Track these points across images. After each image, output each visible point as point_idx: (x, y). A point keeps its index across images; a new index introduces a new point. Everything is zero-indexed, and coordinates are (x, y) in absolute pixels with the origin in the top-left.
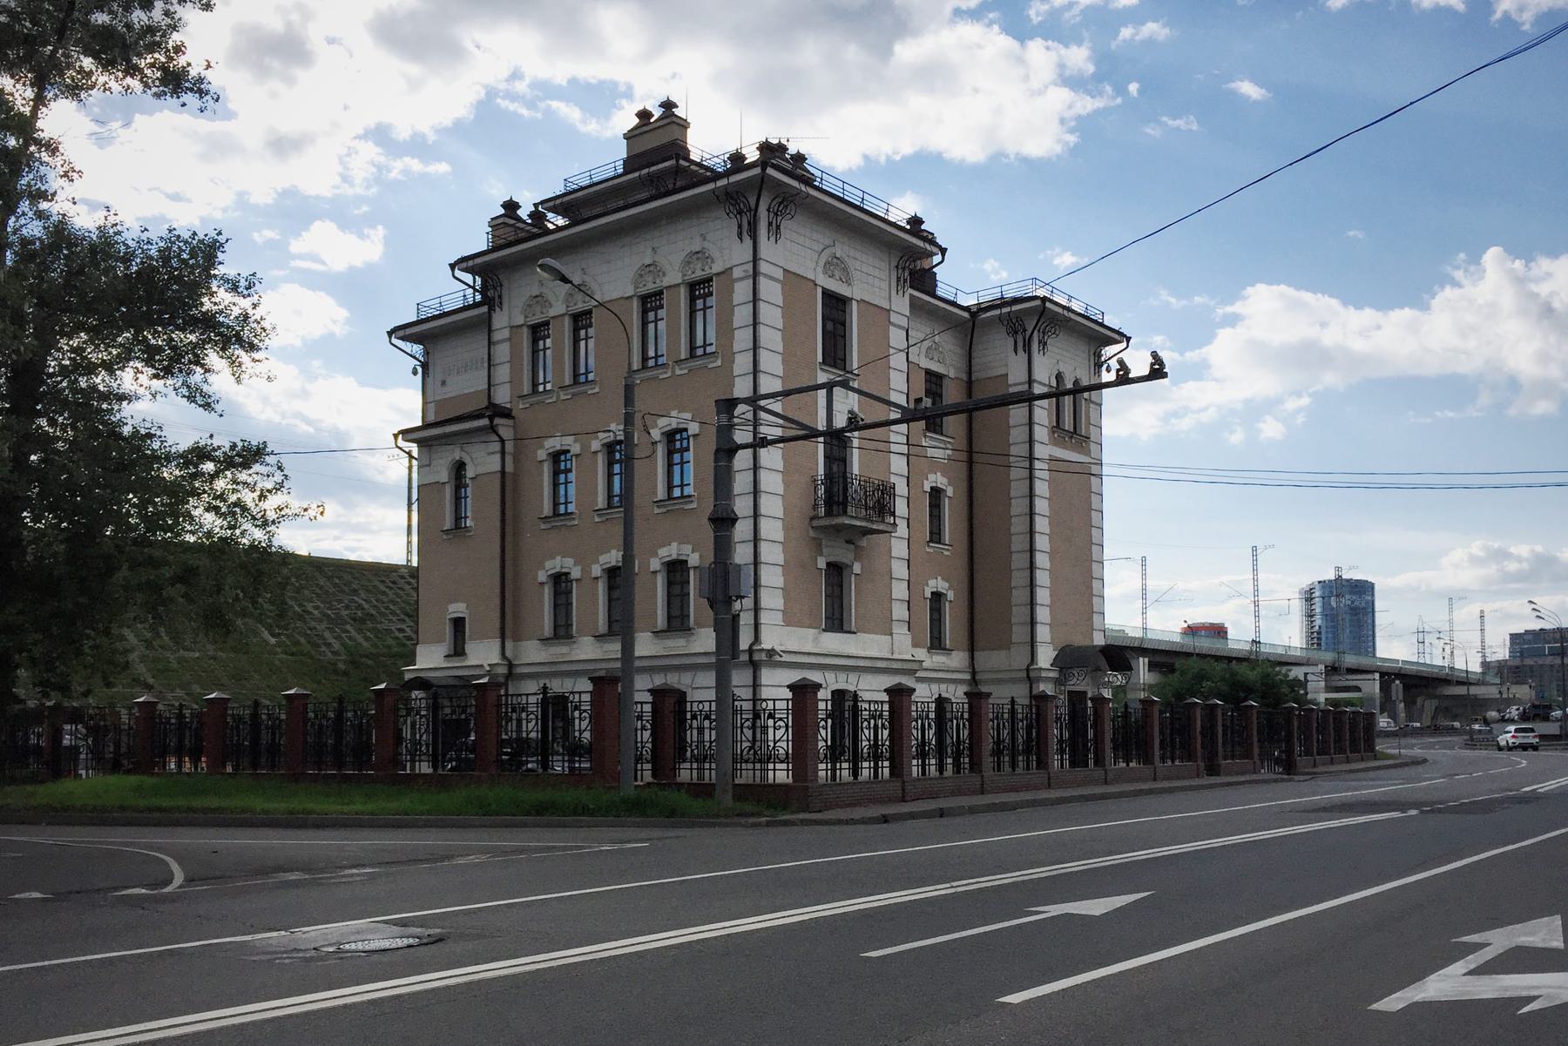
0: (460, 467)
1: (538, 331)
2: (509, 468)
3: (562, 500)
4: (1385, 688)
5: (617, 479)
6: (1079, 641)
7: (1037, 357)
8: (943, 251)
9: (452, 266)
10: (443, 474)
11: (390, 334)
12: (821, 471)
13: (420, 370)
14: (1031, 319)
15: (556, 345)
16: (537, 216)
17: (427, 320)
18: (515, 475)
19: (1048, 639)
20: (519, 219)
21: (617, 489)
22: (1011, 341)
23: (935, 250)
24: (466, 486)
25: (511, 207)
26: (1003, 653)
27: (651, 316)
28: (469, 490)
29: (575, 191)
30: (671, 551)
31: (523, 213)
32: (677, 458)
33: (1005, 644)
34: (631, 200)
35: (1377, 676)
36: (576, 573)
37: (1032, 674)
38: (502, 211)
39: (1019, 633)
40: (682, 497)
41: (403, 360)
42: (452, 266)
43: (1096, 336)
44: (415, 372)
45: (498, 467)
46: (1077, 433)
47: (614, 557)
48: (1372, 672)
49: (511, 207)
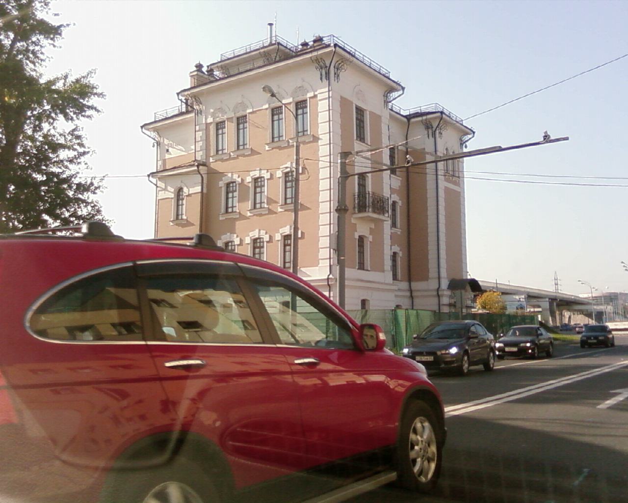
0: (180, 190)
1: (220, 126)
2: (205, 191)
3: (180, 213)
4: (551, 304)
5: (289, 190)
6: (457, 277)
7: (438, 139)
8: (403, 89)
9: (178, 94)
10: (170, 194)
11: (142, 127)
12: (357, 191)
13: (156, 144)
14: (433, 122)
15: (288, 116)
16: (211, 71)
17: (160, 121)
18: (206, 194)
19: (446, 276)
20: (203, 72)
21: (289, 196)
22: (426, 132)
23: (399, 88)
24: (183, 199)
25: (199, 67)
26: (426, 282)
27: (220, 132)
28: (184, 202)
29: (225, 60)
30: (255, 234)
31: (204, 69)
32: (230, 195)
33: (426, 278)
34: (241, 70)
35: (547, 299)
36: (266, 238)
37: (440, 293)
38: (195, 69)
39: (433, 273)
40: (232, 212)
41: (147, 141)
42: (178, 94)
43: (465, 132)
44: (154, 146)
45: (200, 191)
46: (455, 176)
47: (287, 230)
48: (545, 298)
49: (199, 67)
